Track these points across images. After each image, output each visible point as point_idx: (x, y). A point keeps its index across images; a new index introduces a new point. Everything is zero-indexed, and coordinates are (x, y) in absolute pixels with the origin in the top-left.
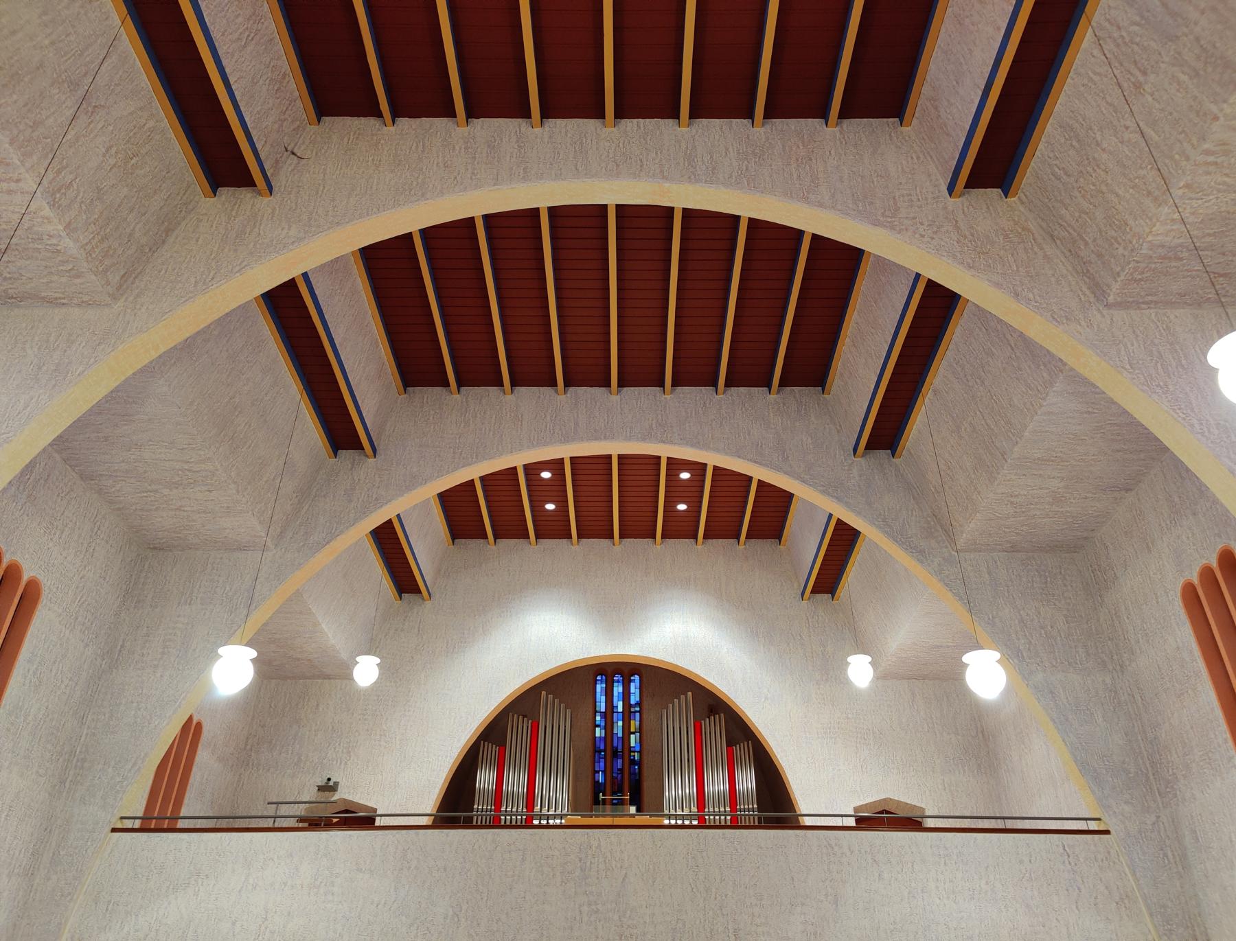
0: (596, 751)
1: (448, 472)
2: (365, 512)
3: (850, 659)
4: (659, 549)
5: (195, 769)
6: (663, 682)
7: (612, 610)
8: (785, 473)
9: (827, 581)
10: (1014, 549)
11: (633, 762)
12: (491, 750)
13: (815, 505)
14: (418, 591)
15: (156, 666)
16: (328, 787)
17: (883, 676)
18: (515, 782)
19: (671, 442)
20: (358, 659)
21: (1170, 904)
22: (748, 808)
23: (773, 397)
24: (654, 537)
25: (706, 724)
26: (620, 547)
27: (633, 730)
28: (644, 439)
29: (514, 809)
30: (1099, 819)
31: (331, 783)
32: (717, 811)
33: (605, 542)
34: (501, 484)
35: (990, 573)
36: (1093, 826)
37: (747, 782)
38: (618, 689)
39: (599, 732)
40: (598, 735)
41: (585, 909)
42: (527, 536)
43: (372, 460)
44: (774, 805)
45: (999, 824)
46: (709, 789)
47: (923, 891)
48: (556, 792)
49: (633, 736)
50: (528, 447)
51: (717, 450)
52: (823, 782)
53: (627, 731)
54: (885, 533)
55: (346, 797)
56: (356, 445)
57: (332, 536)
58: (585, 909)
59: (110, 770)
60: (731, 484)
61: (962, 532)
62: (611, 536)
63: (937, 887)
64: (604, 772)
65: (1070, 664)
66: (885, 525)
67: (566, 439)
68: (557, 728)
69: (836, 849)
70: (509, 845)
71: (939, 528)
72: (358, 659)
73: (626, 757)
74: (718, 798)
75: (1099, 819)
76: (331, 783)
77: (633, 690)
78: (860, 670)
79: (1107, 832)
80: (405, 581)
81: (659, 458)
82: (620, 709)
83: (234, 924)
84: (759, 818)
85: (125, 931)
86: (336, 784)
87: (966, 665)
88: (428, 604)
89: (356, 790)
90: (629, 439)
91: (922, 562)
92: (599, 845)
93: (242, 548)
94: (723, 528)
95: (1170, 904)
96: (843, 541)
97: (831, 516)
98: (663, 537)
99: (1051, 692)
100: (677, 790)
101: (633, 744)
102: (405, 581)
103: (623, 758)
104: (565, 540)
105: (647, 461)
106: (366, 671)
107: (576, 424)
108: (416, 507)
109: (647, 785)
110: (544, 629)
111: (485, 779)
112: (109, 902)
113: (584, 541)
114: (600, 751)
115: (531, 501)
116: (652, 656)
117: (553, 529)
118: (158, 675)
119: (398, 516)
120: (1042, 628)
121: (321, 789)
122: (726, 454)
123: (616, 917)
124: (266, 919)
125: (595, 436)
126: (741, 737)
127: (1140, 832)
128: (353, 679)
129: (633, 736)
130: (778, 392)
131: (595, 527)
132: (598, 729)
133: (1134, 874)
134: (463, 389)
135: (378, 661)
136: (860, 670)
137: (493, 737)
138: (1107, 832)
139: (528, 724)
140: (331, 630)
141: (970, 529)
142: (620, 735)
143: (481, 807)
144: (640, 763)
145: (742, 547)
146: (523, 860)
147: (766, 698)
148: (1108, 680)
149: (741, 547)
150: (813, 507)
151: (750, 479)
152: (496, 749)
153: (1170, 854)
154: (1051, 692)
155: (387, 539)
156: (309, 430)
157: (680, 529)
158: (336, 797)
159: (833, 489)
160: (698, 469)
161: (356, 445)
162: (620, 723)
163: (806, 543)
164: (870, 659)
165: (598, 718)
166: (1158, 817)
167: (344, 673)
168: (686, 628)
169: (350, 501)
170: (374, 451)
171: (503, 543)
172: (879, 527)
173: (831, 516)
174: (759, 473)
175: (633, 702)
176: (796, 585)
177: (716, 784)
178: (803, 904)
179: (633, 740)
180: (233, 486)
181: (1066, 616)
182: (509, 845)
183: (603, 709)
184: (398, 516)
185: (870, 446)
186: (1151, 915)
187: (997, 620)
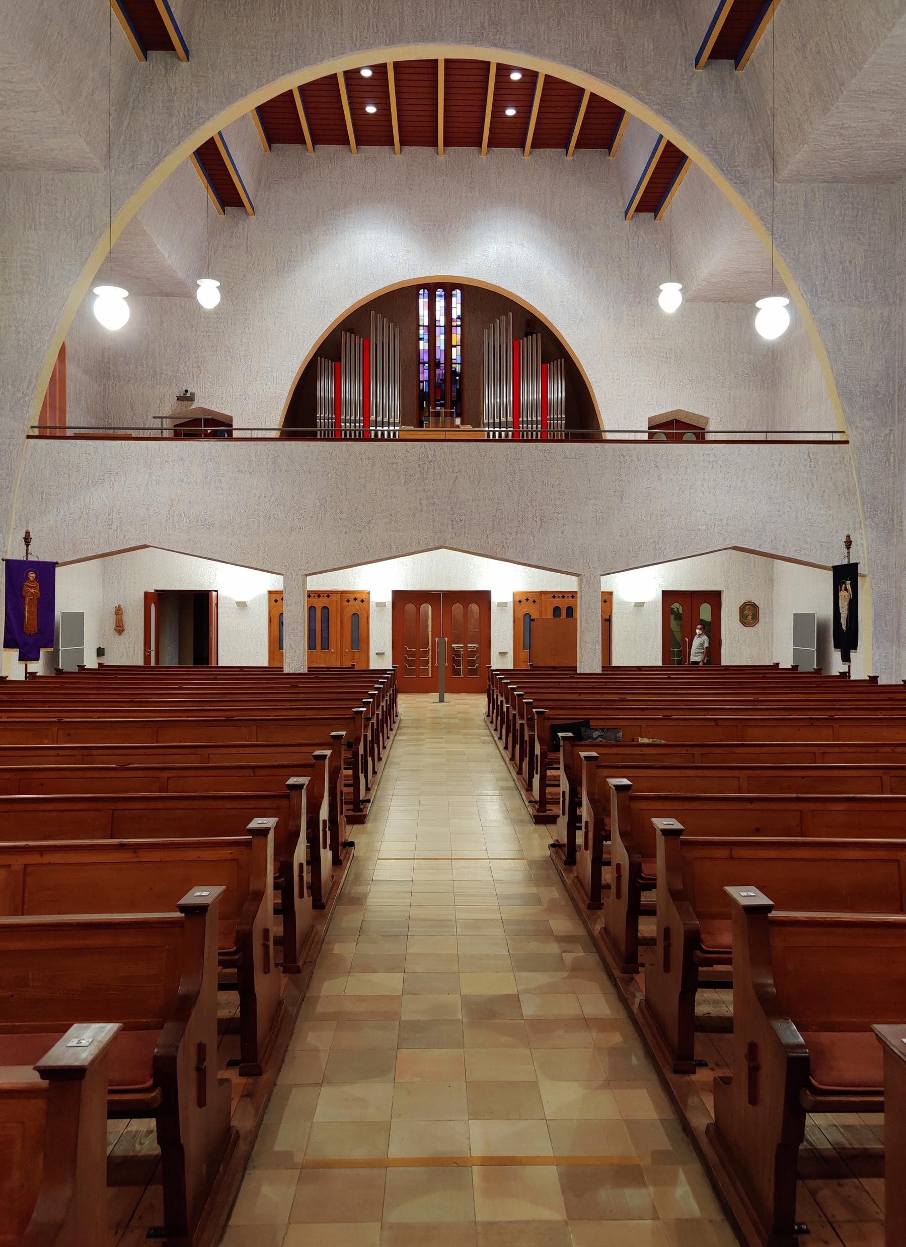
1: (268, 81)
2: (188, 129)
3: (662, 287)
4: (487, 161)
5: (68, 382)
6: (486, 304)
7: (438, 227)
8: (623, 88)
9: (652, 200)
10: (836, 179)
12: (327, 365)
13: (647, 123)
14: (241, 205)
15: (22, 292)
16: (186, 398)
17: (690, 299)
18: (352, 390)
19: (504, 46)
20: (199, 282)
21: (880, 496)
22: (558, 418)
24: (479, 145)
25: (525, 342)
26: (446, 157)
27: (454, 343)
28: (474, 42)
29: (351, 418)
30: (843, 432)
31: (188, 395)
32: (531, 419)
33: (429, 150)
34: (321, 92)
35: (805, 206)
36: (837, 437)
37: (558, 392)
38: (440, 304)
40: (421, 347)
41: (424, 502)
42: (347, 142)
43: (184, 64)
44: (580, 418)
45: (761, 437)
46: (523, 398)
47: (690, 488)
48: (388, 400)
49: (454, 349)
50: (351, 50)
51: (552, 57)
52: (622, 407)
53: (449, 346)
54: (713, 160)
55: (203, 406)
56: (166, 45)
57: (159, 158)
58: (424, 502)
59: (10, 387)
60: (562, 94)
61: (788, 162)
62: (435, 144)
63: (702, 485)
65: (857, 298)
66: (715, 152)
67: (392, 40)
69: (627, 457)
70: (361, 454)
71: (768, 154)
72: (199, 282)
74: (532, 406)
75: (843, 432)
76: (188, 395)
77: (454, 305)
79: (847, 442)
80: (226, 193)
81: (489, 63)
82: (442, 323)
83: (147, 509)
84: (566, 435)
85: (62, 513)
86: (193, 394)
87: (758, 309)
88: (253, 218)
89: (211, 400)
90: (459, 41)
91: (743, 194)
93: (72, 169)
94: (552, 137)
95: (880, 496)
96: (671, 162)
97: (661, 137)
98: (490, 145)
99: (833, 325)
100: (495, 398)
101: (454, 357)
102: (226, 193)
104: (386, 148)
105: (474, 65)
106: (208, 293)
108: (233, 120)
109: (467, 395)
111: (324, 388)
112: (42, 493)
113: (407, 148)
114: (424, 363)
115: (349, 97)
116: (475, 277)
117: (373, 134)
118: (26, 301)
119: (220, 133)
120: (841, 262)
121: (179, 398)
122: (562, 62)
123: (449, 508)
124: (172, 506)
125: (423, 37)
126: (555, 354)
127: (873, 442)
128: (195, 298)
131: (419, 135)
132: (421, 342)
133: (859, 473)
135: (218, 284)
136: (670, 297)
137: (328, 352)
138: (847, 442)
139: (359, 341)
140: (169, 253)
141: (796, 159)
142: (443, 348)
143: (324, 416)
145: (570, 158)
146: (373, 466)
147: (581, 320)
148: (886, 313)
149: (569, 158)
150: (644, 126)
151: (582, 90)
152: (332, 364)
153: (892, 459)
154: (833, 325)
155: (210, 158)
157: (508, 137)
158: (194, 406)
159: (665, 109)
160: (530, 76)
161: (166, 45)
162: (443, 337)
163: (635, 161)
164: (680, 286)
165: (421, 332)
166: (891, 430)
167: (189, 294)
168: (508, 250)
169: (171, 115)
171: (323, 148)
172: (708, 154)
173: (661, 137)
174: (592, 85)
175: (454, 316)
176: (620, 204)
177: (531, 393)
179: (456, 353)
180: (57, 106)
181: (866, 251)
182: (361, 454)
183: (426, 324)
184: (220, 133)
185: (716, 55)
186: (863, 504)
187: (801, 256)
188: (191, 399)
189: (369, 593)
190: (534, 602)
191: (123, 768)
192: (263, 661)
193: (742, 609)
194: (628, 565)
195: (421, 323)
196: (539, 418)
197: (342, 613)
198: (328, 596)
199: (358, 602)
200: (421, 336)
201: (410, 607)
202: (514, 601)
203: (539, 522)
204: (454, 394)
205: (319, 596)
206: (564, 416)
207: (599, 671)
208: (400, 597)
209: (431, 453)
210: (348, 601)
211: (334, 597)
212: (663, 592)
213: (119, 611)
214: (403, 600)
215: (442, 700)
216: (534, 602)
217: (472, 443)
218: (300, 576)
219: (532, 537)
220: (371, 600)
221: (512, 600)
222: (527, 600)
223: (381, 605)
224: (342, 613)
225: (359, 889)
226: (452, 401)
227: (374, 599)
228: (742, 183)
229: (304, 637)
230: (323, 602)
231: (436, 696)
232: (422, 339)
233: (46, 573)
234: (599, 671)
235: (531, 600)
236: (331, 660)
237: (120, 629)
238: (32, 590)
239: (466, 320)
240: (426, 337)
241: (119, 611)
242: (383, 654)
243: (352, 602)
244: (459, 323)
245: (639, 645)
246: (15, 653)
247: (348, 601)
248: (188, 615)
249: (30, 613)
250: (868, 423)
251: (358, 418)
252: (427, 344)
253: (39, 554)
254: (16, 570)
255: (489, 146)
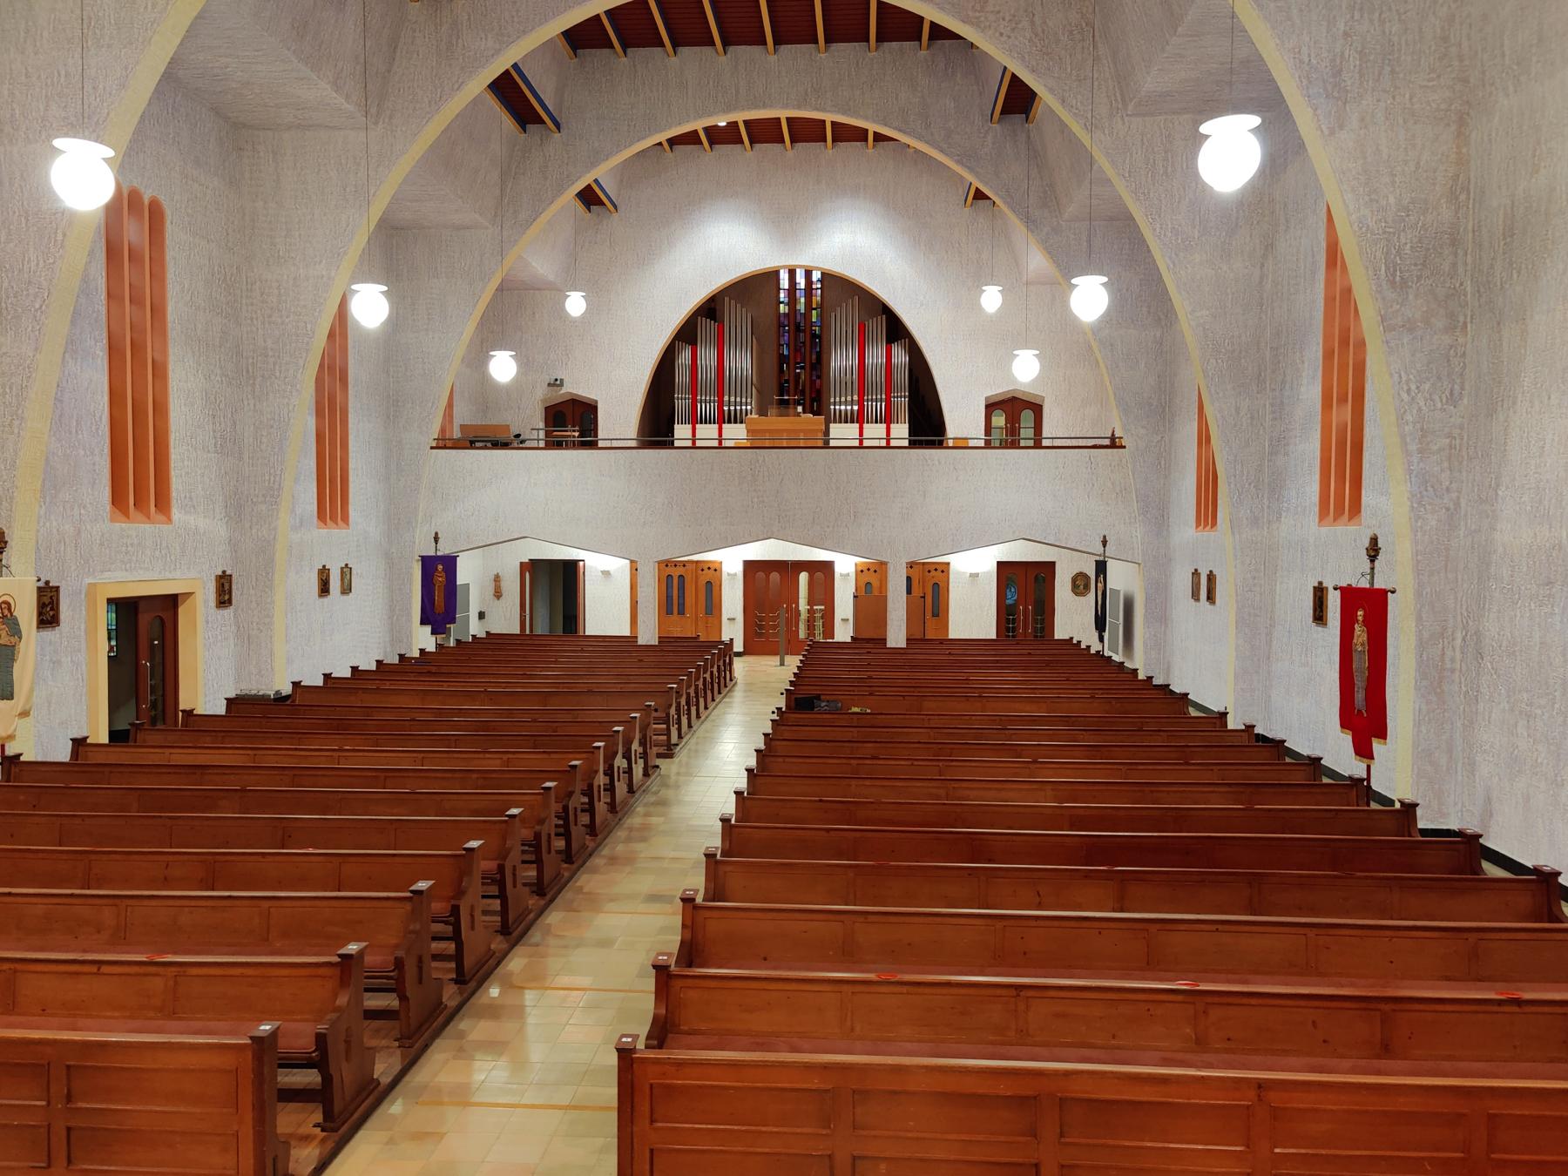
0: (780, 325)
7: (787, 220)
10: (1111, 219)
11: (814, 336)
23: (924, 52)
33: (777, 147)
39: (783, 309)
68: (736, 318)
78: (992, 298)
106: (575, 304)
107: (737, 92)
110: (724, 245)
130: (929, 46)
134: (629, 50)
144: (820, 337)
156: (507, 122)
165: (782, 295)
168: (851, 241)
170: (558, 126)
188: (562, 385)
191: (535, 721)
192: (625, 631)
193: (1074, 580)
201: (761, 575)
207: (904, 645)
208: (751, 567)
211: (689, 566)
212: (999, 563)
213: (497, 579)
215: (782, 664)
225: (670, 793)
228: (1030, 222)
231: (777, 658)
233: (450, 562)
234: (904, 645)
236: (682, 628)
237: (498, 594)
238: (440, 579)
241: (497, 579)
245: (972, 615)
246: (428, 629)
248: (558, 583)
249: (439, 597)
250: (1143, 431)
253: (445, 549)
254: (428, 564)
255: (878, 40)
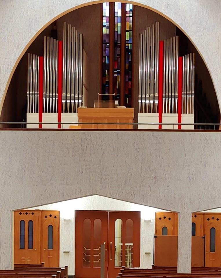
0: (103, 43)
11: (127, 50)
27: (127, 29)
39: (105, 31)
41: (84, 167)
49: (127, 33)
58: (84, 167)
64: (108, 57)
69: (209, 141)
70: (46, 138)
73: (123, 46)
92: (91, 138)
101: (127, 39)
103: (120, 47)
111: (34, 65)
114: (106, 43)
123: (99, 171)
129: (127, 33)
132: (104, 28)
142: (119, 32)
144: (131, 51)
146: (53, 145)
147: (204, 29)
162: (119, 24)
165: (105, 21)
178: (189, 166)
182: (46, 138)
183: (108, 15)
189: (59, 212)
190: (170, 219)
194: (208, 206)
195: (104, 15)
196: (177, 94)
197: (42, 225)
198: (33, 214)
199: (53, 218)
200: (104, 24)
201: (88, 221)
202: (156, 219)
203: (154, 180)
204: (127, 65)
205: (27, 214)
206: (193, 92)
208: (80, 215)
209: (89, 138)
210: (46, 217)
211: (36, 214)
214: (81, 216)
216: (170, 219)
217: (114, 132)
218: (9, 212)
219: (149, 189)
220: (61, 216)
221: (154, 218)
222: (165, 218)
223: (68, 221)
224: (42, 225)
226: (125, 70)
227: (63, 216)
229: (11, 248)
230: (30, 217)
232: (105, 26)
235: (167, 218)
236: (31, 258)
239: (136, 13)
240: (108, 24)
242: (68, 252)
243: (49, 217)
244: (131, 15)
247: (46, 217)
251: (54, 94)
252: (108, 30)
